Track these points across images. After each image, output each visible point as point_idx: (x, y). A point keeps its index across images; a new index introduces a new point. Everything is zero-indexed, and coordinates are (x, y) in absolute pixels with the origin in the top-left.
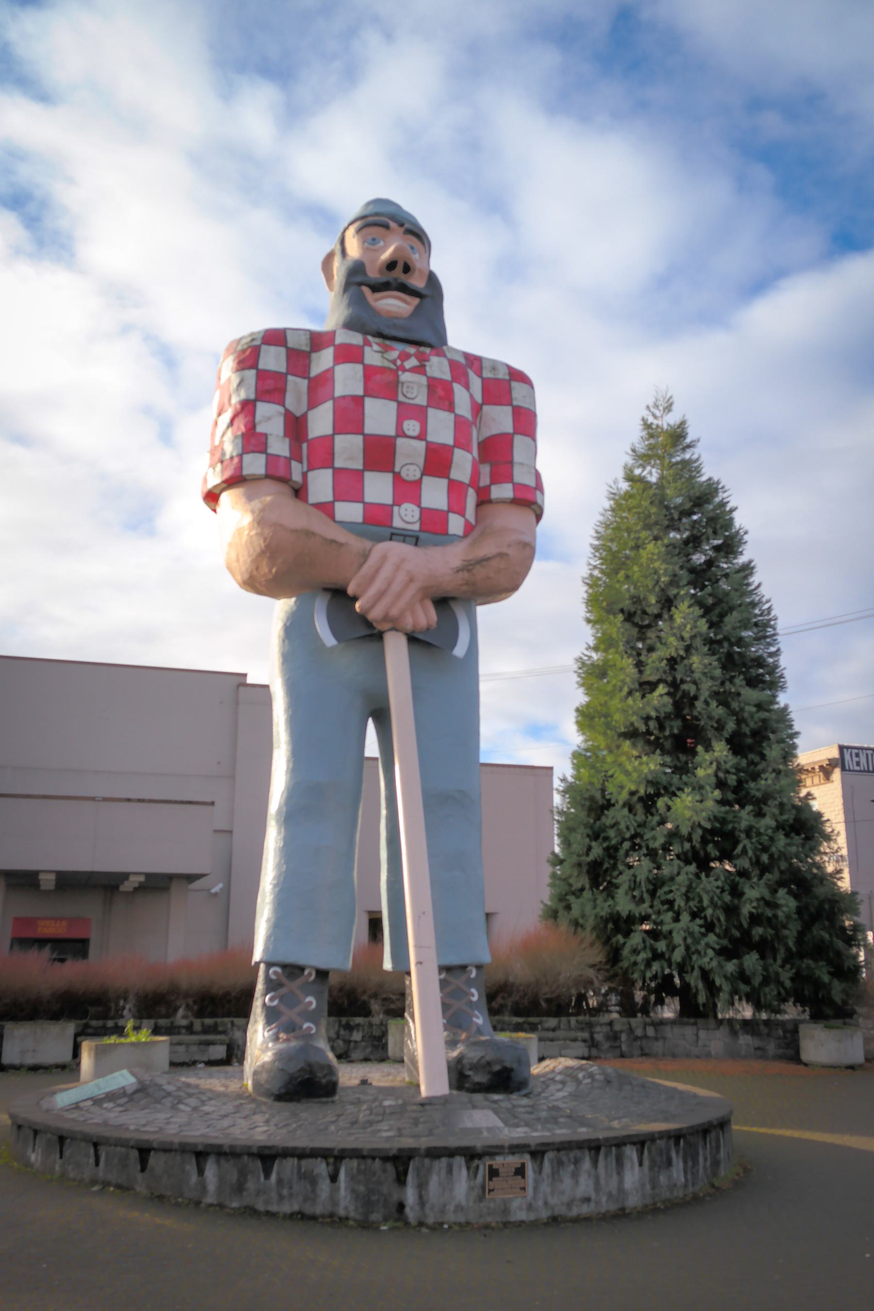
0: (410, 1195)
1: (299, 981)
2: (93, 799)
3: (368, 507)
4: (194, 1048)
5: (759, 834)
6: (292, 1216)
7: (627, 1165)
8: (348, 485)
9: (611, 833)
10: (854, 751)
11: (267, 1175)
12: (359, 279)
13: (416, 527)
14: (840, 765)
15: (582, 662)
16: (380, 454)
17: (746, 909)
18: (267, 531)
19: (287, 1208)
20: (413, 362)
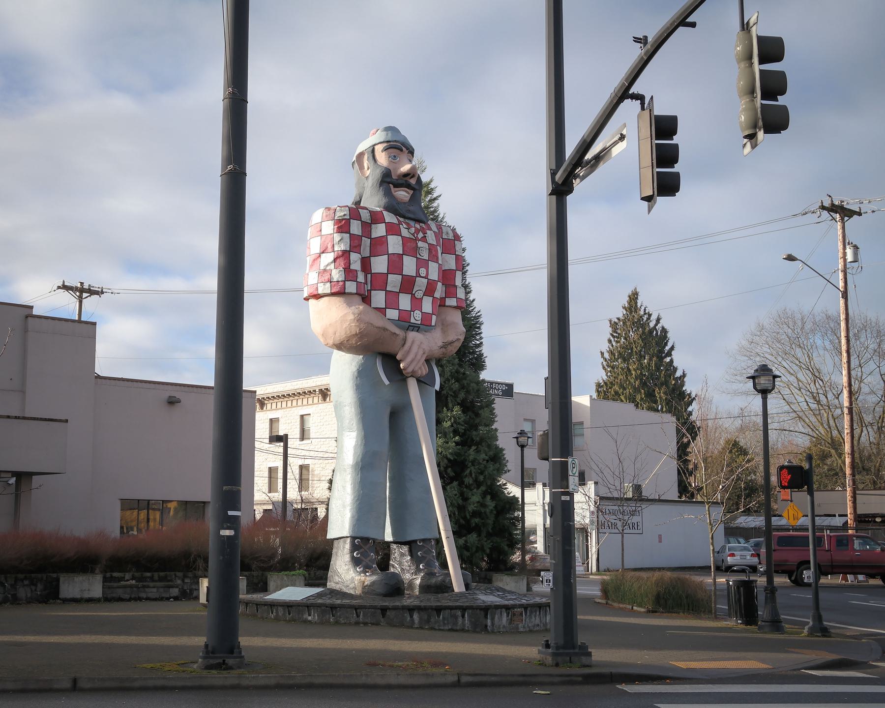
0: (489, 622)
4: (161, 590)
5: (479, 464)
6: (449, 630)
8: (392, 301)
11: (439, 617)
12: (388, 180)
13: (419, 322)
17: (471, 508)
18: (362, 325)
19: (447, 628)
20: (420, 235)
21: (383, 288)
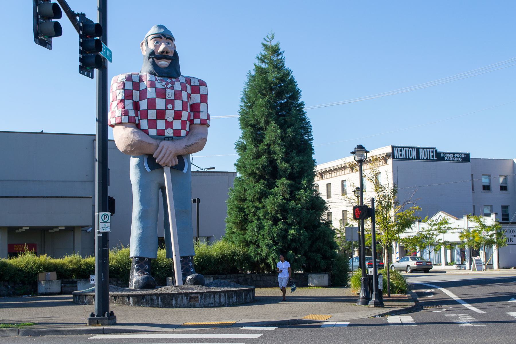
1: (143, 262)
2: (43, 197)
3: (158, 130)
7: (222, 297)
9: (246, 210)
10: (399, 149)
13: (172, 135)
14: (392, 156)
15: (237, 144)
16: (161, 114)
20: (170, 85)
21: (146, 117)
